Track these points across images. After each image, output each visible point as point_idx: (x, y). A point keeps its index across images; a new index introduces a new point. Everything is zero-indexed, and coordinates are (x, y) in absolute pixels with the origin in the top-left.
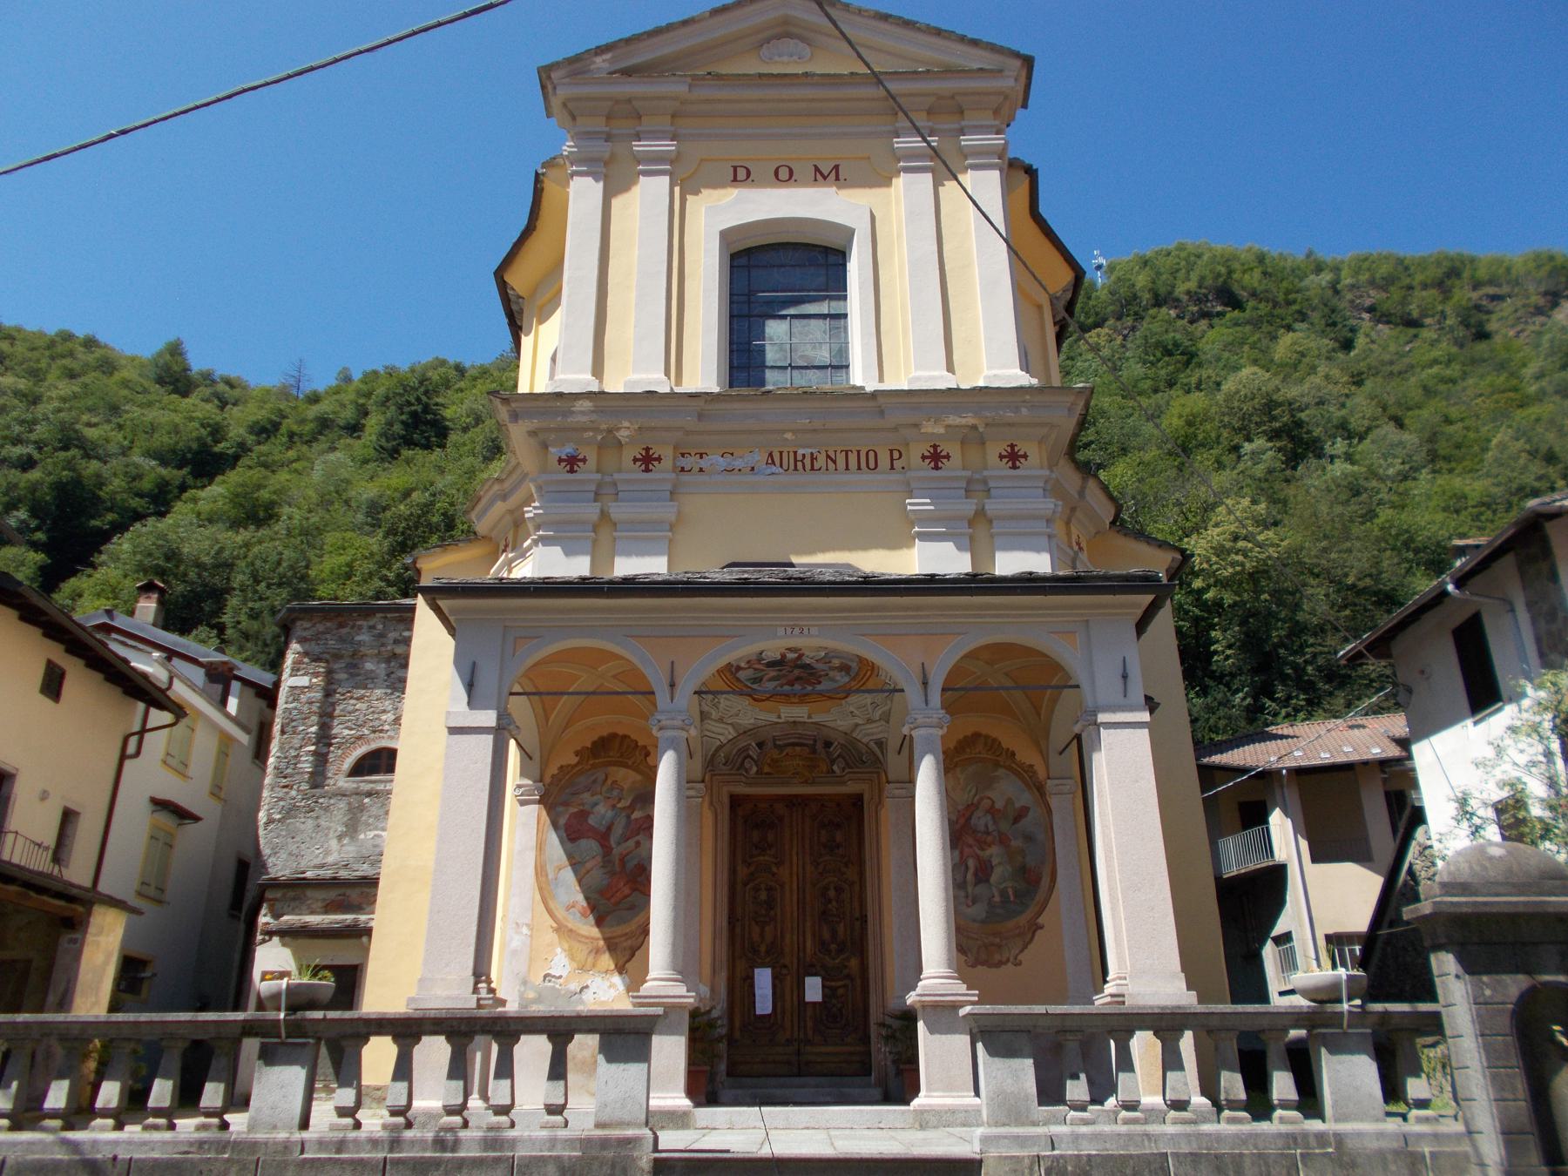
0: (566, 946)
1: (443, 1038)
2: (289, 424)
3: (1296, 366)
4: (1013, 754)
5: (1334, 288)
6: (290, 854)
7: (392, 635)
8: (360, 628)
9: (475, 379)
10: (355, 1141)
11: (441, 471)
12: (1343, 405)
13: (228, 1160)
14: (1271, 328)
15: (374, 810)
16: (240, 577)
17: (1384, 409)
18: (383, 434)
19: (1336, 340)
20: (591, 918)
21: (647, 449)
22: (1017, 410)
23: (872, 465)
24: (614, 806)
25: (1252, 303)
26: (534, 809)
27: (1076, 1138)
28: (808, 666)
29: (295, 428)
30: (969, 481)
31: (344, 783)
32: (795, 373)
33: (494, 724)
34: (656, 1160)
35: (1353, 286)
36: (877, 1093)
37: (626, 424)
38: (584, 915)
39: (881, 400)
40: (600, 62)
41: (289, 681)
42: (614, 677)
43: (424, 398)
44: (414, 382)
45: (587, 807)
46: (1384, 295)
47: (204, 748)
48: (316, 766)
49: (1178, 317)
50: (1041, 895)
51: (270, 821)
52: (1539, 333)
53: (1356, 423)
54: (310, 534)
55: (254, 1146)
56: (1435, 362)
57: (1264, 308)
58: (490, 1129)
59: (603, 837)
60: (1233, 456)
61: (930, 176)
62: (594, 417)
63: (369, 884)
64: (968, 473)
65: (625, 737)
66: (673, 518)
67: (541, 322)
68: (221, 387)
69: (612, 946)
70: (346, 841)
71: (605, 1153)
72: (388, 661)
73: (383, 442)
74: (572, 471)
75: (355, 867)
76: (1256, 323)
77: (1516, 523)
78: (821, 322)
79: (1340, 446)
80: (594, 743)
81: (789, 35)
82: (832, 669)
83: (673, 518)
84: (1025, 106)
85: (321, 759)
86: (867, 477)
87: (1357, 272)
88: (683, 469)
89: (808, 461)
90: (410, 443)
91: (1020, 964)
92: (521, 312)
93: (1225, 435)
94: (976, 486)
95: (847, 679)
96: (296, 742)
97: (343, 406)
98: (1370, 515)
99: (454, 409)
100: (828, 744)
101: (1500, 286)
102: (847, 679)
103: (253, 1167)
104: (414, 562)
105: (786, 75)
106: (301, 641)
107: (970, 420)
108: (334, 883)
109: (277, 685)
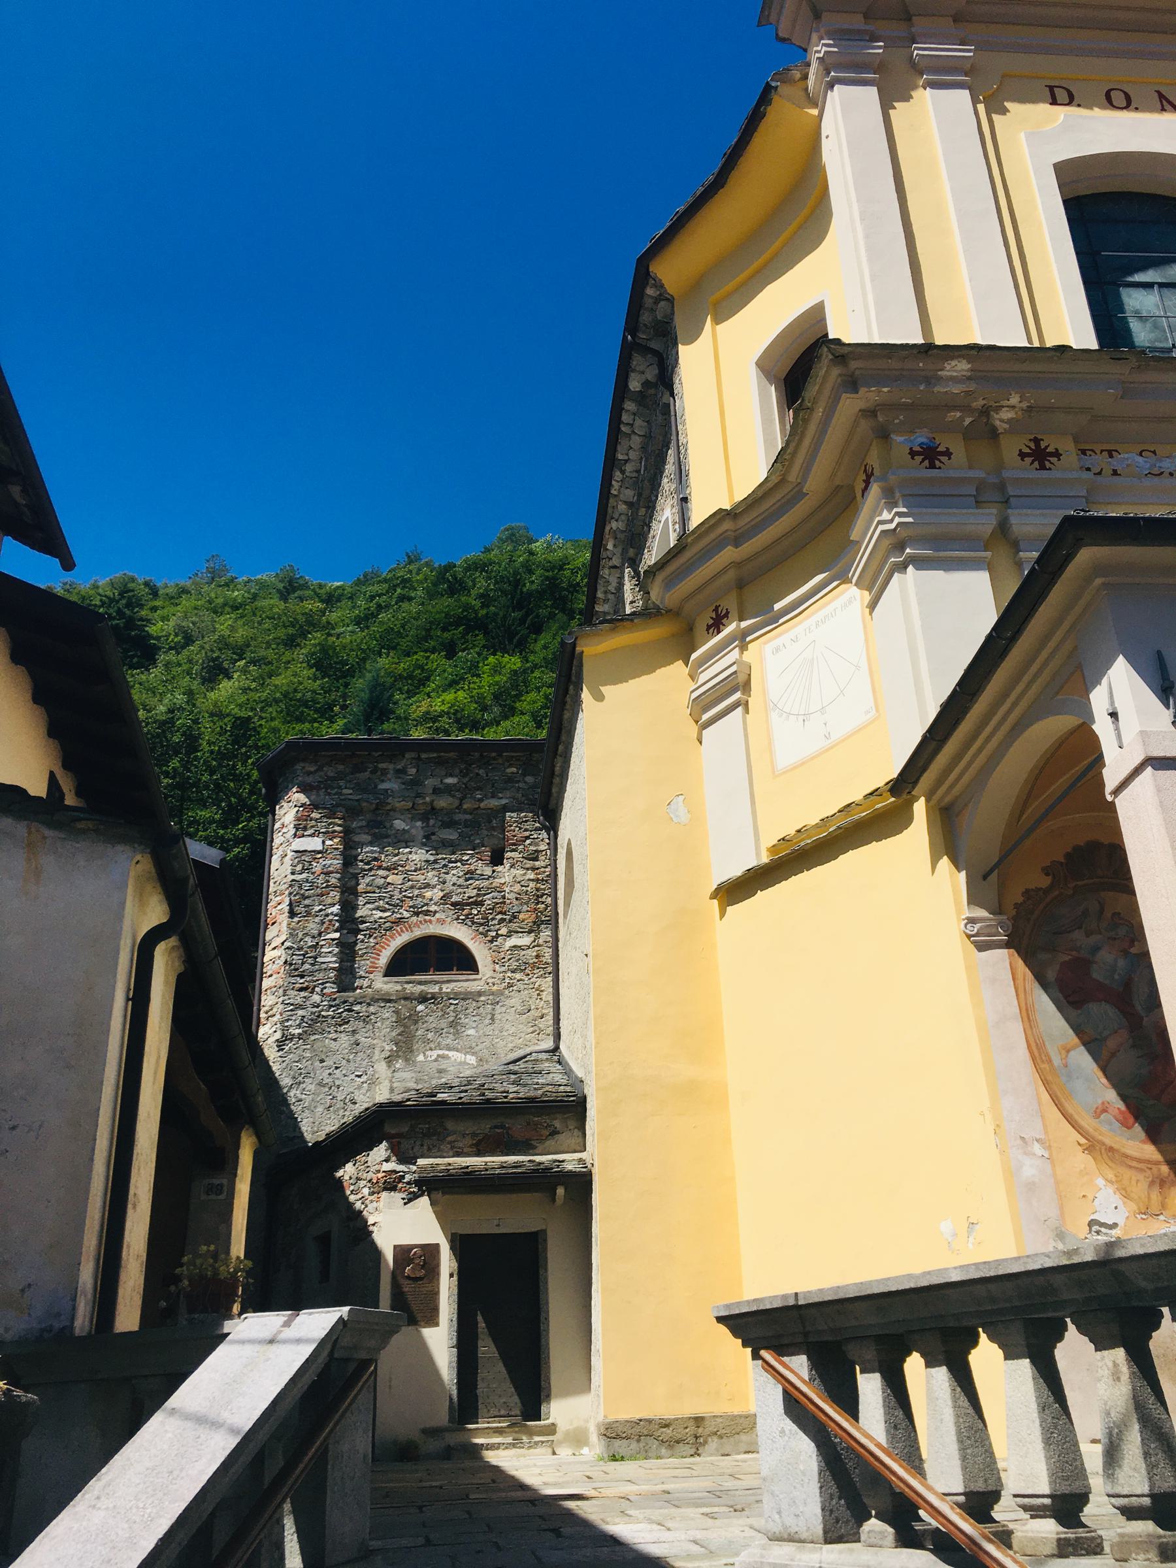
0: (1111, 1176)
6: (321, 1084)
7: (430, 783)
8: (384, 772)
26: (1001, 958)
38: (1124, 1124)
43: (128, 612)
48: (341, 961)
62: (972, 386)
63: (570, 1109)
67: (718, 320)
70: (399, 1064)
72: (425, 818)
77: (161, 1018)
80: (1068, 856)
85: (348, 952)
96: (312, 926)
106: (304, 789)
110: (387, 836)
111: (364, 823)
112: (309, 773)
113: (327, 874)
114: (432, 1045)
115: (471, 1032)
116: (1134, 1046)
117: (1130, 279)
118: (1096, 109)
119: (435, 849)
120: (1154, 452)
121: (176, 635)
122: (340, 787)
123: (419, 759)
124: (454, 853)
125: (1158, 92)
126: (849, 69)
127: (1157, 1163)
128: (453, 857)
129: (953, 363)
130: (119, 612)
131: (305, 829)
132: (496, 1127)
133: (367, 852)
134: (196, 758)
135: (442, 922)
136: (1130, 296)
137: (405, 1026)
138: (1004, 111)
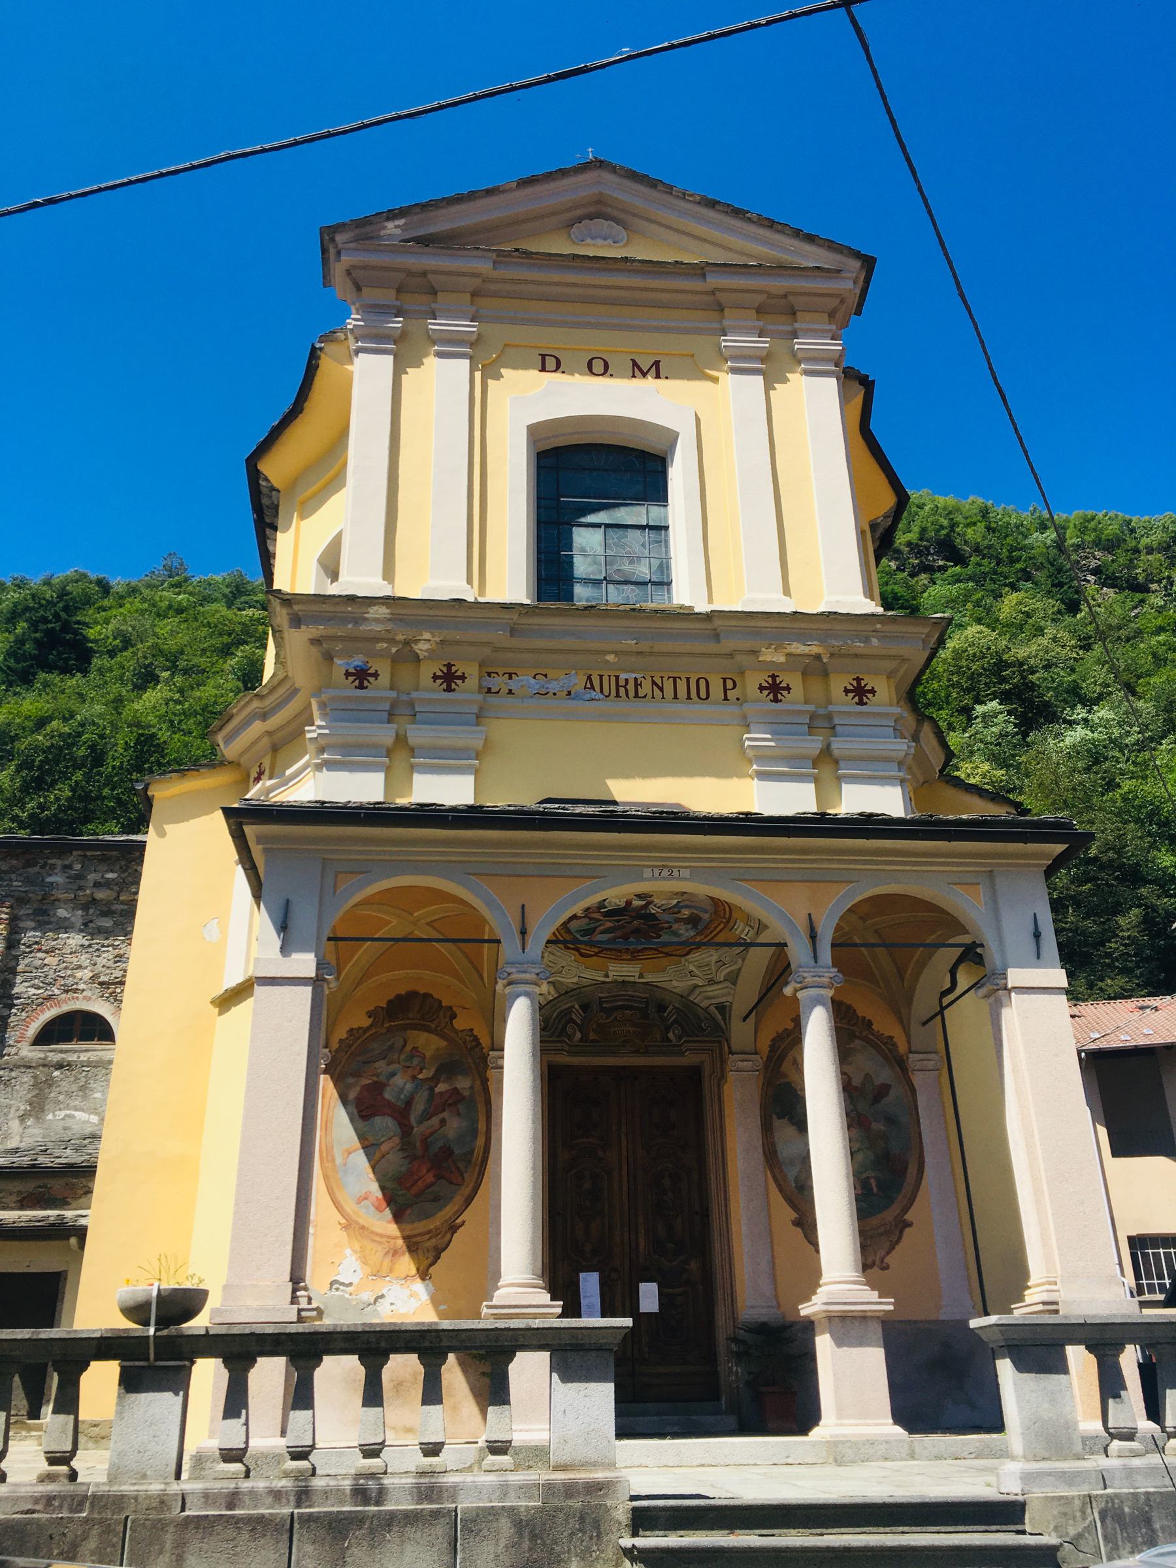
0: (357, 1247)
1: (414, 1357)
4: (870, 1023)
5: (1060, 544)
7: (92, 877)
8: (53, 867)
9: (122, 597)
10: (252, 1493)
11: (81, 697)
12: (1073, 670)
13: (86, 1520)
14: (994, 587)
15: (65, 1086)
19: (1063, 601)
20: (388, 1212)
21: (449, 666)
22: (866, 640)
23: (703, 694)
24: (414, 1078)
25: (974, 559)
27: (1130, 1472)
28: (653, 917)
30: (813, 716)
31: (28, 1052)
32: (611, 587)
33: (313, 975)
34: (634, 1509)
35: (1078, 547)
36: (732, 1420)
37: (427, 636)
39: (717, 622)
40: (392, 228)
44: (49, 594)
45: (382, 1079)
46: (1110, 558)
49: (898, 569)
50: (907, 1188)
53: (1090, 689)
55: (119, 1501)
56: (1160, 630)
57: (988, 565)
58: (422, 1474)
59: (401, 1114)
60: (963, 718)
61: (759, 379)
62: (390, 626)
64: (811, 708)
65: (427, 996)
66: (479, 744)
67: (303, 517)
69: (412, 1246)
71: (571, 1502)
72: (85, 907)
73: (12, 662)
74: (361, 687)
75: (57, 1152)
78: (639, 532)
79: (1080, 713)
80: (390, 1002)
81: (607, 217)
82: (677, 920)
84: (858, 312)
86: (699, 708)
87: (1083, 530)
88: (489, 691)
90: (50, 668)
91: (887, 1268)
92: (276, 508)
93: (954, 695)
94: (821, 722)
95: (692, 933)
98: (1111, 785)
99: (99, 629)
100: (662, 1008)
102: (692, 933)
103: (120, 1528)
105: (603, 258)
107: (815, 650)
108: (33, 1172)
110: (50, 923)
111: (30, 911)
114: (62, 1106)
115: (98, 1095)
117: (583, 520)
118: (577, 375)
119: (92, 934)
120: (546, 676)
121: (115, 638)
122: (11, 880)
123: (85, 856)
124: (107, 939)
125: (633, 360)
126: (375, 340)
127: (395, 1238)
128: (106, 942)
129: (376, 608)
130: (56, 616)
132: (40, 1187)
133: (30, 936)
134: (100, 774)
135: (88, 999)
136: (580, 535)
137: (40, 1089)
138: (498, 376)
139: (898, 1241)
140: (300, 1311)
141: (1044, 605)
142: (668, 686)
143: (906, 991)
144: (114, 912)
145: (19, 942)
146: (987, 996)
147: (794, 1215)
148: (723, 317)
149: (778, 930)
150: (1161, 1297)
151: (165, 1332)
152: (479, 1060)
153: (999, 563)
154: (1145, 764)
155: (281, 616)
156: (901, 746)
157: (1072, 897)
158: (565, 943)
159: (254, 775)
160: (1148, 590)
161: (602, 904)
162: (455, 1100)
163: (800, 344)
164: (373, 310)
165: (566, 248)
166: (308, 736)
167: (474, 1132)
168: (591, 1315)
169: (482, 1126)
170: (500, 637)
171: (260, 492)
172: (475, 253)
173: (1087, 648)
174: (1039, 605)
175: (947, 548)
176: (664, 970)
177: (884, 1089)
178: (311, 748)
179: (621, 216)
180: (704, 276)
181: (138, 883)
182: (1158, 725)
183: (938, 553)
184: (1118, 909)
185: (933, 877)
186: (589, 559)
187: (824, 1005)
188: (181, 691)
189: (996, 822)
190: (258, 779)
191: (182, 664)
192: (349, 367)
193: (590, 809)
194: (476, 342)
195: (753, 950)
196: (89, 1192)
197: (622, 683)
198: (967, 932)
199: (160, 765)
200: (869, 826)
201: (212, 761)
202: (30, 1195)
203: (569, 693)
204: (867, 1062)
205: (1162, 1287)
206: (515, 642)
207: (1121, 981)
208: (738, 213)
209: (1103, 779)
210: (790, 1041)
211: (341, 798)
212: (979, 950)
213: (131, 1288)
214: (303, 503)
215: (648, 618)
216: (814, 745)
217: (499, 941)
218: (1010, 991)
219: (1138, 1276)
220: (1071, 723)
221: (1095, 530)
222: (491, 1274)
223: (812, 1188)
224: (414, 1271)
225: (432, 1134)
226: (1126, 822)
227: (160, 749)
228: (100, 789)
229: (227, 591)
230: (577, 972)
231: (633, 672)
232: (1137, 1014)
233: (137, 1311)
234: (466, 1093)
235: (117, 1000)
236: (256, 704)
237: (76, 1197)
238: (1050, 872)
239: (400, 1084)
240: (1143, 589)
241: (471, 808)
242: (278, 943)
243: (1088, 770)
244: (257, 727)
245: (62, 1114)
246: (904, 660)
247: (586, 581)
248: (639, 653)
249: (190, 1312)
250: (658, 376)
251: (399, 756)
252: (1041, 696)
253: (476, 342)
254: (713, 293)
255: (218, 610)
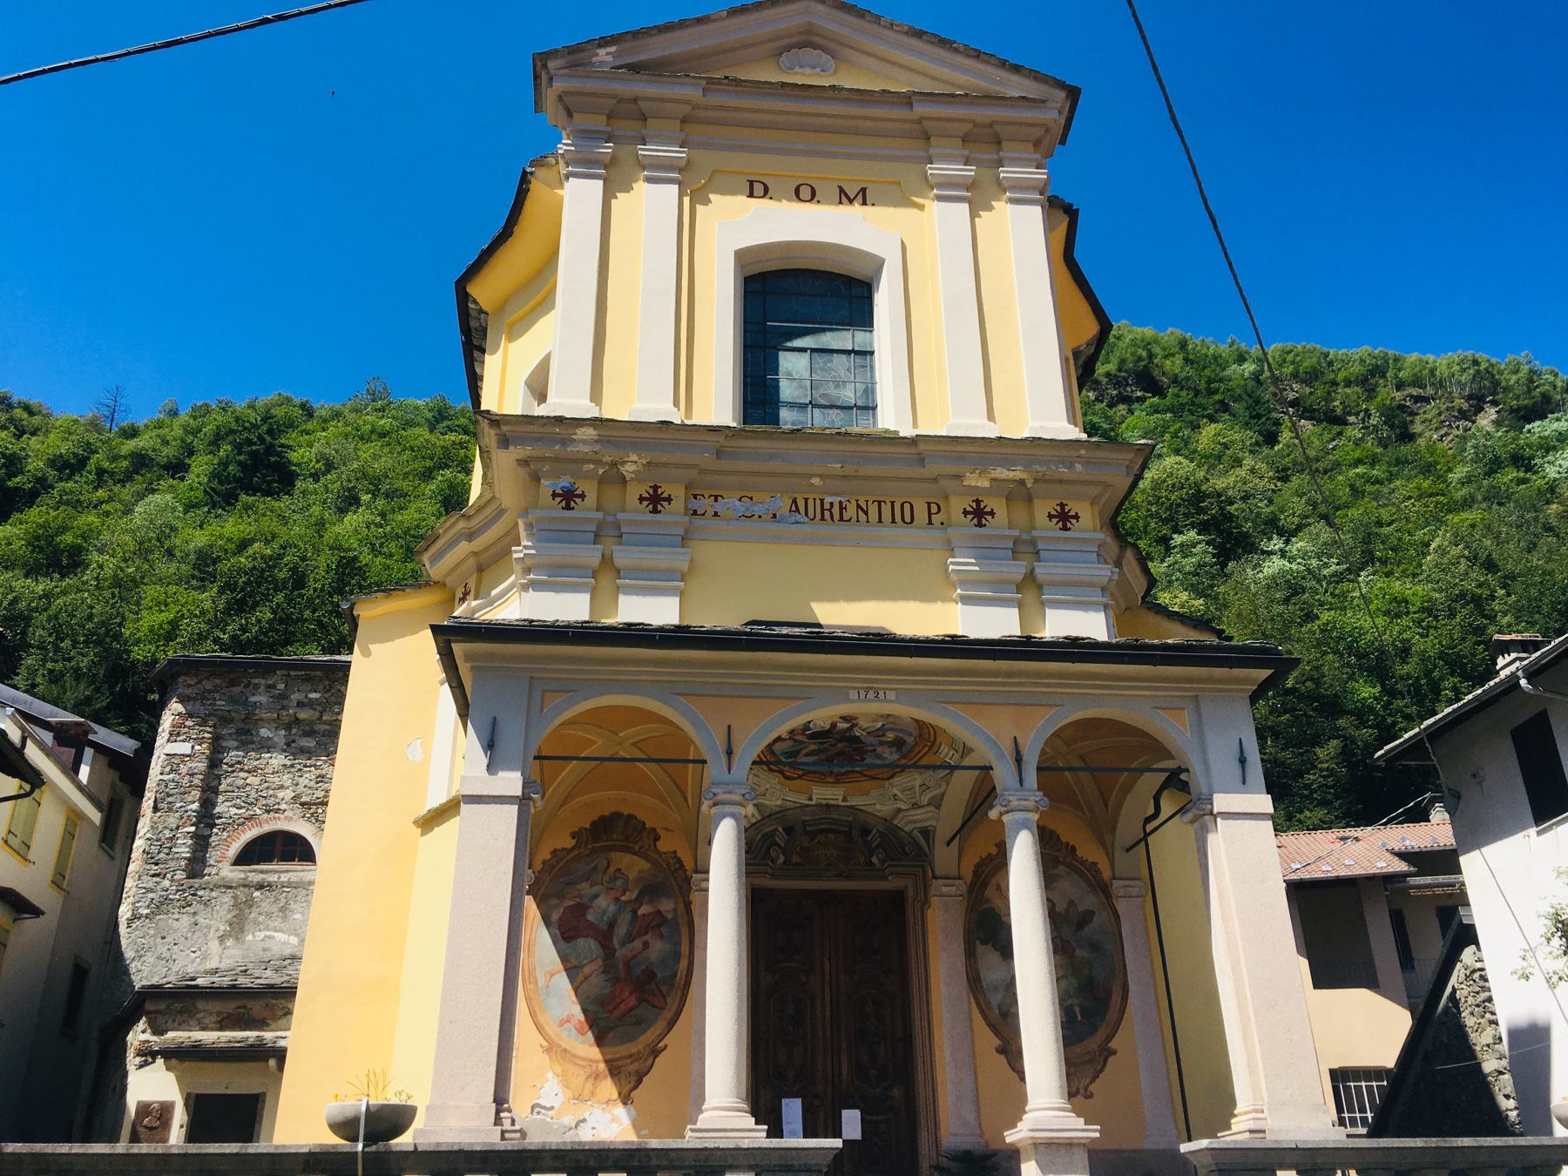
0: (559, 1071)
2: (99, 459)
3: (1218, 458)
4: (1074, 849)
7: (295, 697)
8: (256, 687)
9: (325, 421)
12: (1271, 501)
15: (265, 906)
16: (39, 632)
17: (1315, 505)
18: (214, 476)
19: (1260, 433)
21: (655, 488)
22: (1071, 466)
23: (908, 519)
24: (617, 899)
28: (857, 739)
29: (106, 465)
30: (1017, 541)
32: (816, 411)
33: (519, 793)
37: (634, 457)
39: (922, 447)
40: (604, 55)
41: (164, 747)
42: (634, 744)
43: (268, 438)
44: (253, 417)
45: (585, 900)
46: (1308, 390)
47: (49, 823)
48: (194, 852)
49: (1097, 399)
50: (1112, 1015)
51: (135, 917)
52: (1464, 438)
54: (125, 587)
56: (1358, 462)
59: (604, 936)
60: (1162, 548)
61: (965, 206)
62: (597, 448)
64: (1016, 533)
65: (631, 817)
66: (685, 569)
67: (510, 340)
68: (18, 413)
69: (614, 1069)
72: (288, 727)
73: (215, 484)
75: (257, 973)
76: (1177, 410)
78: (844, 357)
79: (1276, 543)
80: (594, 824)
81: (815, 47)
82: (882, 743)
83: (685, 569)
84: (1063, 142)
85: (201, 843)
86: (902, 532)
88: (695, 512)
89: (836, 510)
90: (251, 489)
91: (1091, 1096)
92: (484, 331)
93: (1153, 525)
94: (1025, 547)
95: (896, 757)
96: (172, 820)
97: (166, 443)
98: (1310, 617)
99: (301, 454)
100: (865, 831)
101: (1423, 387)
102: (896, 757)
104: (351, 608)
105: (811, 86)
107: (1019, 474)
109: (147, 749)
112: (189, 686)
113: (192, 775)
115: (298, 916)
116: (604, 972)
117: (789, 344)
119: (294, 754)
126: (586, 165)
130: (260, 438)
131: (178, 734)
133: (233, 756)
134: (301, 596)
135: (289, 819)
138: (707, 202)
139: (1102, 1070)
140: (503, 1132)
141: (1241, 436)
142: (873, 510)
143: (1111, 810)
144: (316, 732)
145: (221, 761)
146: (1192, 822)
147: (997, 1042)
148: (929, 146)
149: (983, 752)
150: (1364, 1131)
151: (373, 1148)
152: (681, 882)
153: (1196, 393)
154: (1344, 595)
155: (489, 436)
156: (1105, 572)
157: (1271, 728)
158: (767, 763)
159: (459, 595)
160: (1346, 423)
161: (806, 726)
162: (658, 922)
163: (1006, 172)
164: (586, 136)
165: (776, 77)
166: (515, 556)
167: (677, 956)
168: (793, 1135)
169: (685, 949)
170: (707, 460)
171: (468, 315)
172: (686, 80)
173: (1285, 479)
174: (1237, 437)
175: (1144, 379)
176: (867, 793)
177: (1087, 917)
178: (517, 568)
179: (832, 45)
180: (911, 105)
181: (341, 703)
182: (1356, 557)
183: (1137, 384)
184: (1316, 740)
185: (1132, 700)
186: (795, 384)
187: (1029, 829)
188: (383, 515)
189: (1201, 647)
190: (463, 600)
191: (384, 487)
192: (559, 192)
193: (797, 631)
194: (684, 168)
195: (957, 773)
196: (289, 1013)
197: (827, 506)
198: (1172, 757)
199: (361, 587)
200: (1075, 649)
201: (417, 581)
202: (230, 1015)
203: (775, 516)
204: (1071, 888)
205: (1364, 1121)
206: (725, 464)
207: (1320, 813)
208: (944, 43)
209: (1302, 610)
210: (997, 862)
211: (549, 617)
212: (1183, 777)
213: (339, 1103)
214: (511, 326)
215: (852, 442)
216: (1017, 570)
217: (704, 762)
218: (1215, 817)
219: (1339, 1110)
220: (1270, 553)
221: (1293, 363)
222: (697, 1098)
223: (1017, 1015)
224: (615, 1095)
225: (634, 957)
226: (1325, 653)
227: (361, 572)
228: (301, 612)
229: (429, 415)
230: (781, 794)
231: (836, 495)
232: (1339, 844)
233: (345, 1127)
234: (669, 916)
235: (319, 822)
236: (461, 524)
237: (276, 1019)
238: (1254, 698)
239: (603, 906)
240: (1341, 421)
241: (678, 628)
242: (486, 761)
243: (1286, 601)
244: (464, 548)
245: (262, 935)
246: (1107, 486)
247: (792, 405)
248: (845, 477)
249: (399, 1130)
250: (864, 203)
251: (605, 576)
252: (1239, 526)
253: (684, 168)
254: (919, 121)
255: (421, 434)
